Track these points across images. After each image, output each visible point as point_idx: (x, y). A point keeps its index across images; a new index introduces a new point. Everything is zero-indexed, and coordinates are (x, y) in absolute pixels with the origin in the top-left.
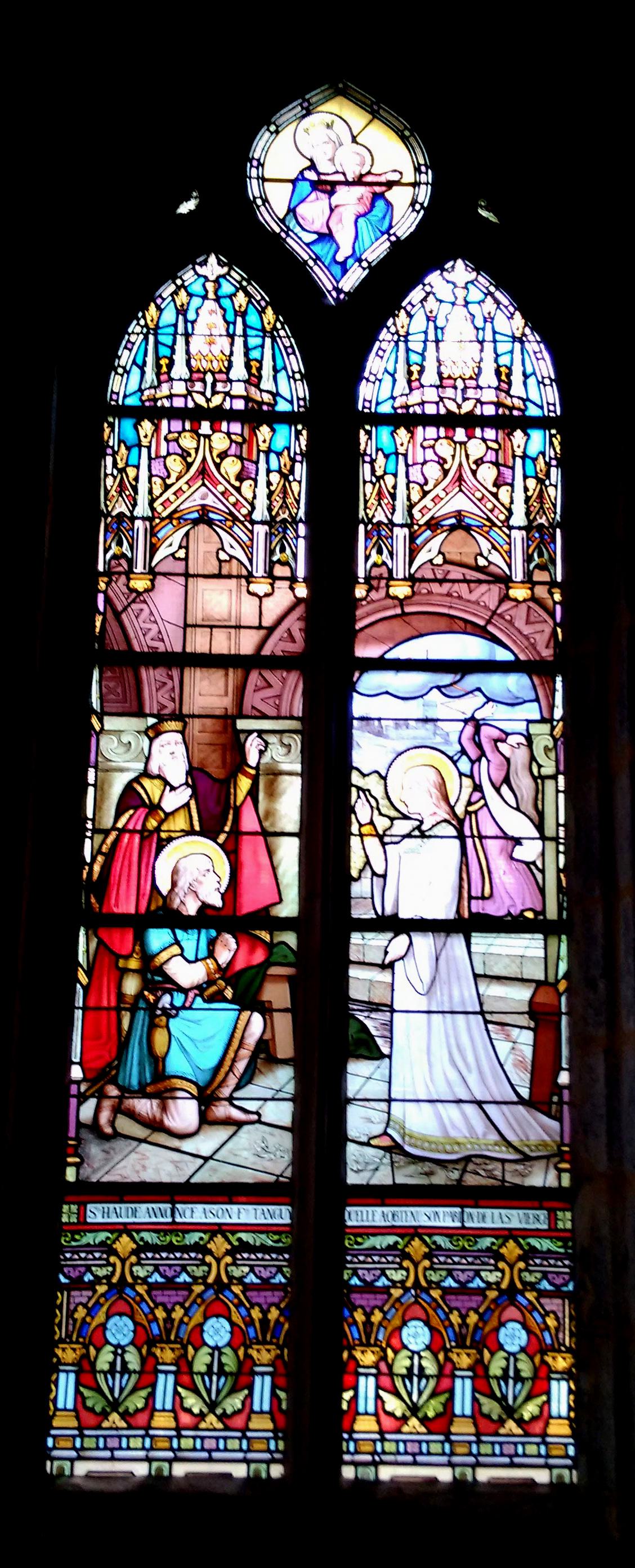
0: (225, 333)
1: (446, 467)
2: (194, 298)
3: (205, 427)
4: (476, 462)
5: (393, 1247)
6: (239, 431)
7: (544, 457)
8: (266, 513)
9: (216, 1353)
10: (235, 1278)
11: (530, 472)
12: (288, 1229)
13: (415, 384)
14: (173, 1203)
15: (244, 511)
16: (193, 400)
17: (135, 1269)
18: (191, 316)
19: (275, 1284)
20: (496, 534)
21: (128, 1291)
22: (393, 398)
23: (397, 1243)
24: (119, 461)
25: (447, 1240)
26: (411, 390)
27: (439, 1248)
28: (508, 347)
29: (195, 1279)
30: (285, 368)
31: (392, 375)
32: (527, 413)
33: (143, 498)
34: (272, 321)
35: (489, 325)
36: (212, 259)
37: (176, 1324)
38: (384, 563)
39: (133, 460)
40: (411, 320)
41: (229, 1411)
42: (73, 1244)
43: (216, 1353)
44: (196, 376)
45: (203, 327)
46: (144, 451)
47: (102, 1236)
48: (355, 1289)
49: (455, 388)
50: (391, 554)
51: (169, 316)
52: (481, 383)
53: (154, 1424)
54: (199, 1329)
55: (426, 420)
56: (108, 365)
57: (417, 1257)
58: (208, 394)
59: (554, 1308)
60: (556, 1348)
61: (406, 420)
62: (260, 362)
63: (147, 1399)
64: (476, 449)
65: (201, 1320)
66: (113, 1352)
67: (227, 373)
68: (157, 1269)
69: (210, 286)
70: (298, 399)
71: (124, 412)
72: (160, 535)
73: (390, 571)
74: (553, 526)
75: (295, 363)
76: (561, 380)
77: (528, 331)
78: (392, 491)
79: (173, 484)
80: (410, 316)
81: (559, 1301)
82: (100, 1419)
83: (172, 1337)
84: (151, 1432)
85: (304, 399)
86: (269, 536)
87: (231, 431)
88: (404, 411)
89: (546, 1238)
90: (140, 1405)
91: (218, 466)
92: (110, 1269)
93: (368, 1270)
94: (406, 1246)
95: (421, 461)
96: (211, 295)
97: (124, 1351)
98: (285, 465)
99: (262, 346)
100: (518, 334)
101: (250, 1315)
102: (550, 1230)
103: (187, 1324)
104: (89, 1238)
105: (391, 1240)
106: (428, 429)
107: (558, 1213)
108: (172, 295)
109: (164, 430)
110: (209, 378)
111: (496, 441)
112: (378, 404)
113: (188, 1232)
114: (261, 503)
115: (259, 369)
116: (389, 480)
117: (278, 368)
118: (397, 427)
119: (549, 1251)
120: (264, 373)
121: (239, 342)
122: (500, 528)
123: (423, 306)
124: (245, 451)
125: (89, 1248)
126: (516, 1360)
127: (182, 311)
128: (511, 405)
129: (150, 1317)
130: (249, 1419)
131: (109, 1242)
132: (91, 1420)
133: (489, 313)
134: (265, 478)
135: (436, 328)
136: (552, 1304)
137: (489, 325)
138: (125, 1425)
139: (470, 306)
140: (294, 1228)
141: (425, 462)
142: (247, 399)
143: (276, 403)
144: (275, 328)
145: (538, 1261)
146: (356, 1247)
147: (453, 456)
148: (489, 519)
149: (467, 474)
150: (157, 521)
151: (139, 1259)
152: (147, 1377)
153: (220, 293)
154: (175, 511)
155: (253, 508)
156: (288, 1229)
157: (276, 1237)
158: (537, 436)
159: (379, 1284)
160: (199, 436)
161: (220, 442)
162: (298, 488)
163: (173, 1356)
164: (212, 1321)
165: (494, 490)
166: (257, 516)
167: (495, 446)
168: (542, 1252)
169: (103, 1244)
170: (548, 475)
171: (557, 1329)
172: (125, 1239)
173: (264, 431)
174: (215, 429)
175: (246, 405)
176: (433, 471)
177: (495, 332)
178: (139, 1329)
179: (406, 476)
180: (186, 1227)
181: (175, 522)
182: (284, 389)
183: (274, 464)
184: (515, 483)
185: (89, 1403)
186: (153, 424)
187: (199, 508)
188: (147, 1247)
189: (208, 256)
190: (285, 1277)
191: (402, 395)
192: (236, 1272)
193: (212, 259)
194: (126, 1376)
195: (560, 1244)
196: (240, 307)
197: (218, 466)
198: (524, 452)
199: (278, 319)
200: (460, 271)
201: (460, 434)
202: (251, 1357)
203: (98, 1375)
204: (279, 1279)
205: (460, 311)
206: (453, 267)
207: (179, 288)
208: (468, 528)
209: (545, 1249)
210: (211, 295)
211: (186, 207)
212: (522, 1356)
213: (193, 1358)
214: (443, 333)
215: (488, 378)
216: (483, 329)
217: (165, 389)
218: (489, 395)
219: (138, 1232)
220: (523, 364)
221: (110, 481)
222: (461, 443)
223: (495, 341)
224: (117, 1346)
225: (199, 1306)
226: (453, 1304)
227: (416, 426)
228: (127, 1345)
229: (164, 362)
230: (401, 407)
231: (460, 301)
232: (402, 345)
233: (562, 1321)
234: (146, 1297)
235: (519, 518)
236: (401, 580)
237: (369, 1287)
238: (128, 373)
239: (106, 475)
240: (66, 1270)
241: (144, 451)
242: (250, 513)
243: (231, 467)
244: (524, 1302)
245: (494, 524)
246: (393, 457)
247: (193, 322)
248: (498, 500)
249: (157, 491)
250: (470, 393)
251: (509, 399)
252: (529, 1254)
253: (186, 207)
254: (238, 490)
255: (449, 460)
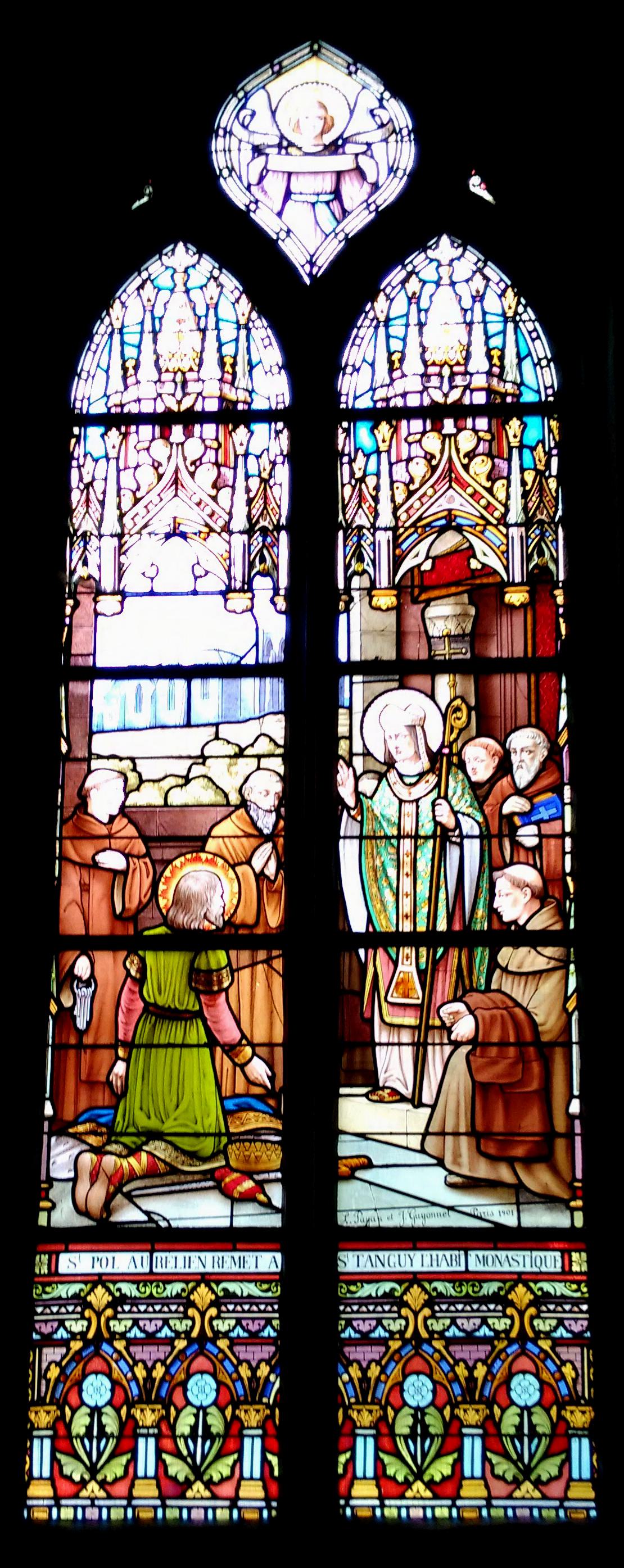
0: (195, 327)
1: (434, 462)
2: (427, 285)
3: (449, 426)
4: (193, 463)
5: (389, 1295)
6: (485, 427)
7: (544, 447)
8: (522, 515)
9: (525, 1413)
10: (437, 1332)
11: (528, 462)
12: (277, 1277)
13: (131, 380)
14: (151, 1252)
15: (497, 514)
16: (429, 395)
17: (215, 1323)
18: (424, 304)
19: (375, 1339)
20: (491, 533)
21: (105, 1347)
22: (373, 390)
23: (393, 1290)
24: (85, 475)
25: (449, 1286)
26: (126, 387)
27: (440, 1295)
28: (500, 327)
29: (392, 1333)
30: (530, 354)
31: (372, 365)
32: (522, 400)
33: (385, 508)
34: (513, 305)
35: (478, 305)
36: (445, 240)
37: (262, 1382)
38: (365, 571)
39: (372, 467)
40: (391, 302)
41: (545, 1477)
42: (45, 1296)
43: (525, 1413)
44: (431, 370)
45: (172, 325)
46: (113, 462)
47: (74, 1288)
48: (351, 1342)
49: (440, 375)
50: (373, 562)
51: (400, 306)
52: (202, 376)
53: (571, 1494)
54: (398, 1388)
55: (409, 413)
56: (70, 372)
57: (416, 1305)
58: (446, 387)
59: (572, 1357)
60: (575, 1400)
61: (117, 420)
62: (502, 350)
63: (453, 1466)
64: (194, 448)
65: (436, 1377)
66: (412, 1415)
67: (466, 365)
68: (239, 1321)
69: (179, 278)
70: (546, 388)
71: (356, 415)
72: (404, 546)
73: (98, 583)
74: (278, 528)
75: (542, 348)
76: (559, 358)
77: (254, 315)
78: (374, 493)
79: (142, 498)
80: (390, 300)
81: (578, 1350)
82: (512, 1487)
83: (369, 1400)
84: (567, 1504)
85: (552, 387)
86: (524, 540)
87: (477, 428)
88: (119, 410)
89: (560, 1281)
90: (447, 1471)
91: (466, 467)
92: (190, 1323)
93: (364, 1320)
94: (404, 1293)
95: (405, 456)
96: (180, 288)
97: (424, 1414)
98: (540, 461)
99: (504, 332)
100: (243, 321)
101: (237, 1371)
102: (563, 1272)
103: (386, 1383)
104: (63, 1291)
105: (387, 1287)
106: (413, 422)
107: (573, 1254)
108: (138, 289)
109: (404, 432)
110: (446, 371)
111: (489, 431)
112: (356, 398)
113: (170, 1282)
114: (516, 505)
115: (501, 358)
116: (371, 481)
117: (523, 355)
118: (108, 429)
119: (563, 1296)
120: (239, 369)
121: (478, 330)
122: (496, 526)
123: (139, 294)
124: (496, 450)
125: (59, 1301)
126: (530, 1414)
127: (413, 299)
128: (503, 391)
129: (234, 1376)
130: (567, 1487)
131: (184, 1295)
132: (394, 1490)
133: (478, 291)
134: (519, 476)
135: (419, 311)
136: (572, 1353)
137: (478, 305)
138: (539, 1495)
139: (457, 286)
140: (283, 1278)
141: (409, 459)
142: (489, 391)
143: (521, 394)
144: (516, 313)
145: (552, 1307)
146: (348, 1295)
147: (169, 458)
148: (207, 525)
149: (184, 476)
150: (401, 530)
151: (116, 1312)
152: (452, 1440)
153: (189, 285)
154: (420, 519)
155: (507, 510)
156: (277, 1277)
157: (265, 1286)
158: (534, 423)
159: (265, 1334)
160: (171, 444)
161: (466, 441)
162: (350, 493)
163: (370, 1418)
164: (412, 1379)
165: (488, 485)
166: (512, 518)
167: (488, 437)
168: (556, 1297)
169: (76, 1296)
170: (548, 465)
171: (575, 1381)
172: (100, 1290)
173: (514, 426)
174: (188, 434)
175: (488, 397)
176: (147, 476)
177: (484, 313)
178: (223, 1389)
179: (384, 474)
180: (220, 1277)
181: (419, 530)
182: (529, 377)
183: (528, 462)
184: (512, 477)
185: (499, 1471)
186: (391, 426)
187: (445, 513)
188: (123, 1299)
189: (175, 246)
190: (275, 1330)
191: (382, 386)
192: (437, 1326)
193: (445, 240)
194: (536, 1441)
195: (574, 1287)
196: (212, 298)
197: (466, 467)
198: (521, 441)
199: (519, 303)
200: (445, 248)
201: (449, 426)
202: (458, 1417)
203: (398, 1439)
204: (269, 1332)
205: (445, 291)
206: (173, 250)
207: (410, 274)
208: (184, 536)
209: (558, 1294)
210: (446, 281)
211: (476, 185)
212: (537, 1410)
213: (394, 1420)
214: (161, 325)
215: (211, 369)
216: (472, 309)
217: (399, 386)
218: (479, 381)
219: (115, 1282)
220: (517, 346)
221: (348, 490)
222: (450, 436)
223: (485, 322)
224: (417, 1409)
225: (397, 1363)
226: (458, 1356)
227: (399, 420)
228: (428, 1406)
229: (130, 364)
230: (382, 400)
231: (446, 281)
232: (117, 337)
233: (580, 1371)
234: (125, 1353)
235: (515, 515)
236: (385, 589)
237: (365, 1339)
238: (358, 370)
239: (343, 485)
240: (37, 1326)
241: (384, 456)
242: (505, 515)
243: (481, 467)
244: (536, 1351)
245: (489, 523)
246: (374, 458)
247: (426, 311)
248: (493, 496)
249: (400, 498)
250: (459, 380)
251: (502, 384)
252: (541, 1300)
253: (476, 185)
254: (490, 491)
255: (164, 462)
